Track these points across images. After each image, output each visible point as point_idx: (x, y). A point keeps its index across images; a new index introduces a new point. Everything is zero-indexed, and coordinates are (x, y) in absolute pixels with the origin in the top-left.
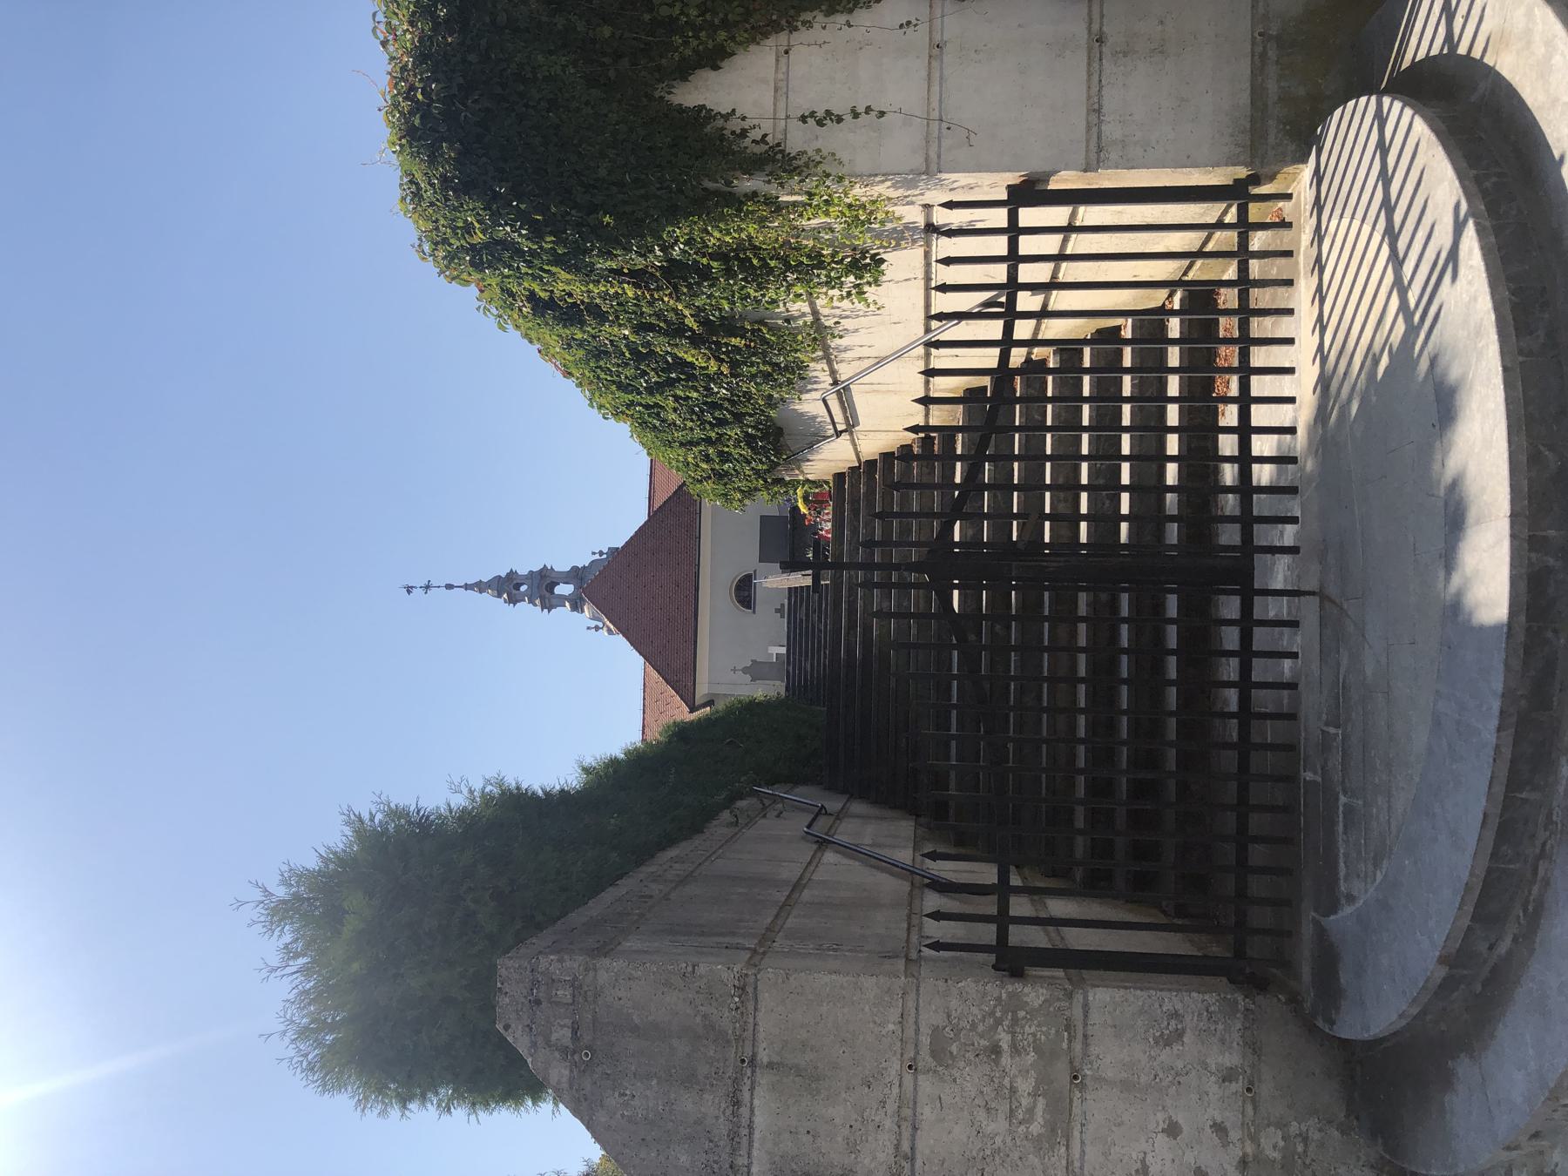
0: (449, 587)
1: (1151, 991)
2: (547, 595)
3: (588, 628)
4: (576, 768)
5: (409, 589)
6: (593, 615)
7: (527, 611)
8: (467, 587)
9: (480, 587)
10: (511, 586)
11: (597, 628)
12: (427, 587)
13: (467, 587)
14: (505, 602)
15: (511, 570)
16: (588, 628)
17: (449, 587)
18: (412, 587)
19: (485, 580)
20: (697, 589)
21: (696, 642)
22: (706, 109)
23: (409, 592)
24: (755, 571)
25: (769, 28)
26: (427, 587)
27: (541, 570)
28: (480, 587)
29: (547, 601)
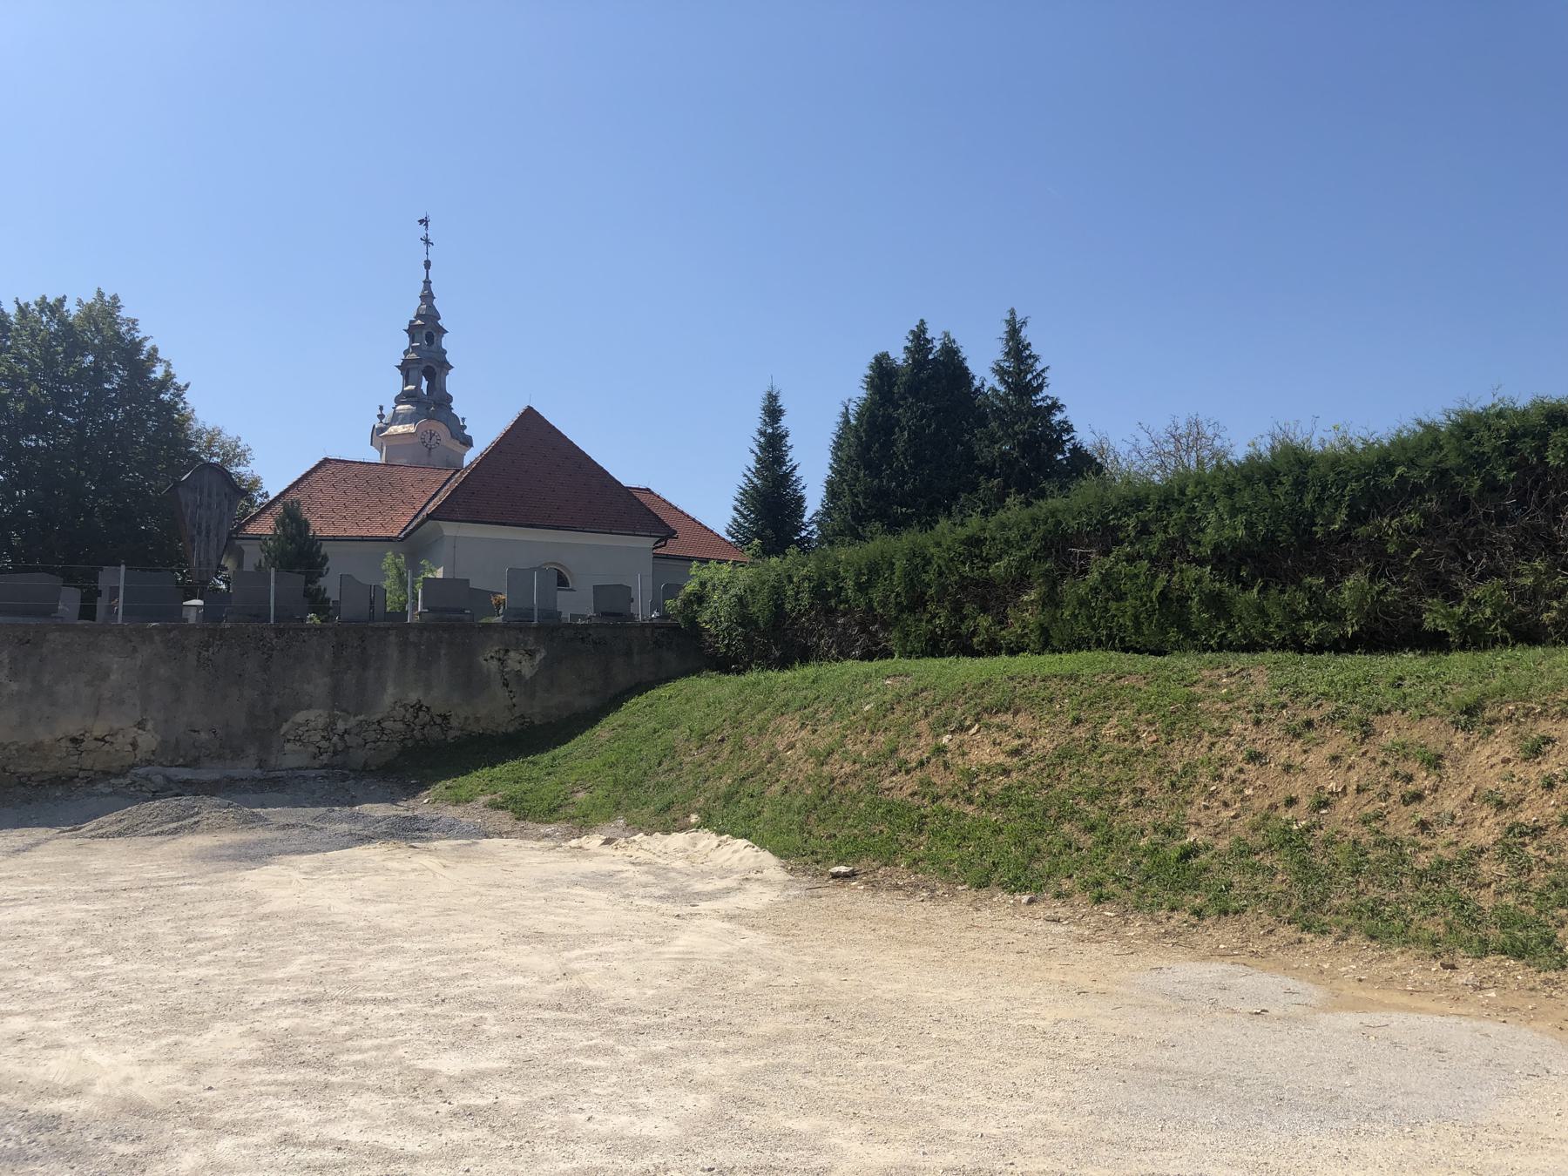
0: (428, 264)
1: (1023, 722)
2: (422, 366)
3: (381, 408)
4: (1376, 435)
5: (425, 222)
6: (399, 414)
7: (399, 345)
8: (427, 283)
9: (427, 297)
10: (430, 330)
11: (381, 416)
12: (427, 242)
13: (427, 283)
14: (411, 322)
15: (100, 294)
16: (381, 408)
17: (428, 264)
18: (426, 225)
19: (435, 302)
20: (558, 528)
21: (504, 524)
22: (1060, 511)
23: (421, 222)
24: (571, 590)
25: (352, 775)
26: (427, 242)
27: (446, 362)
28: (427, 297)
29: (416, 366)
